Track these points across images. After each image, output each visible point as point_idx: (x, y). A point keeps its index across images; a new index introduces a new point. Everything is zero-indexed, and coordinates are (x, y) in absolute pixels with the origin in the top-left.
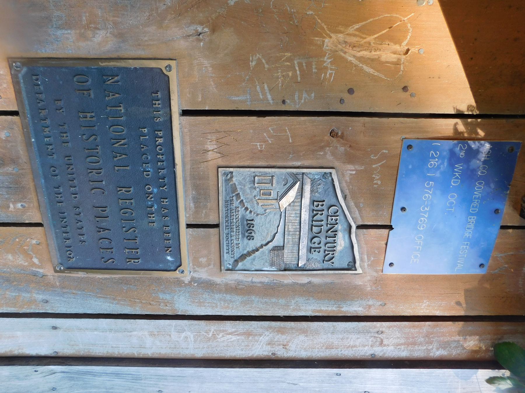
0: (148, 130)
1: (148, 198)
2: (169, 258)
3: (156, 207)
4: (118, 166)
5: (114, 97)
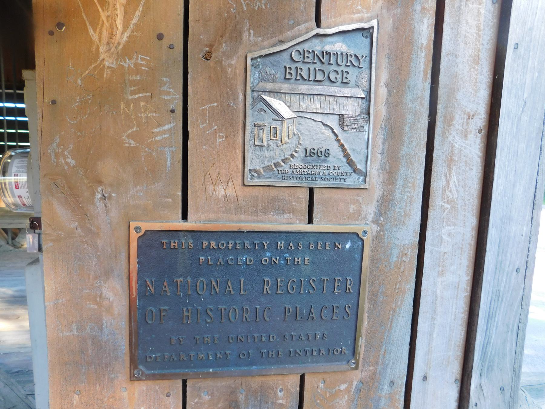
0: (202, 256)
1: (277, 262)
2: (347, 246)
3: (288, 255)
5: (167, 286)
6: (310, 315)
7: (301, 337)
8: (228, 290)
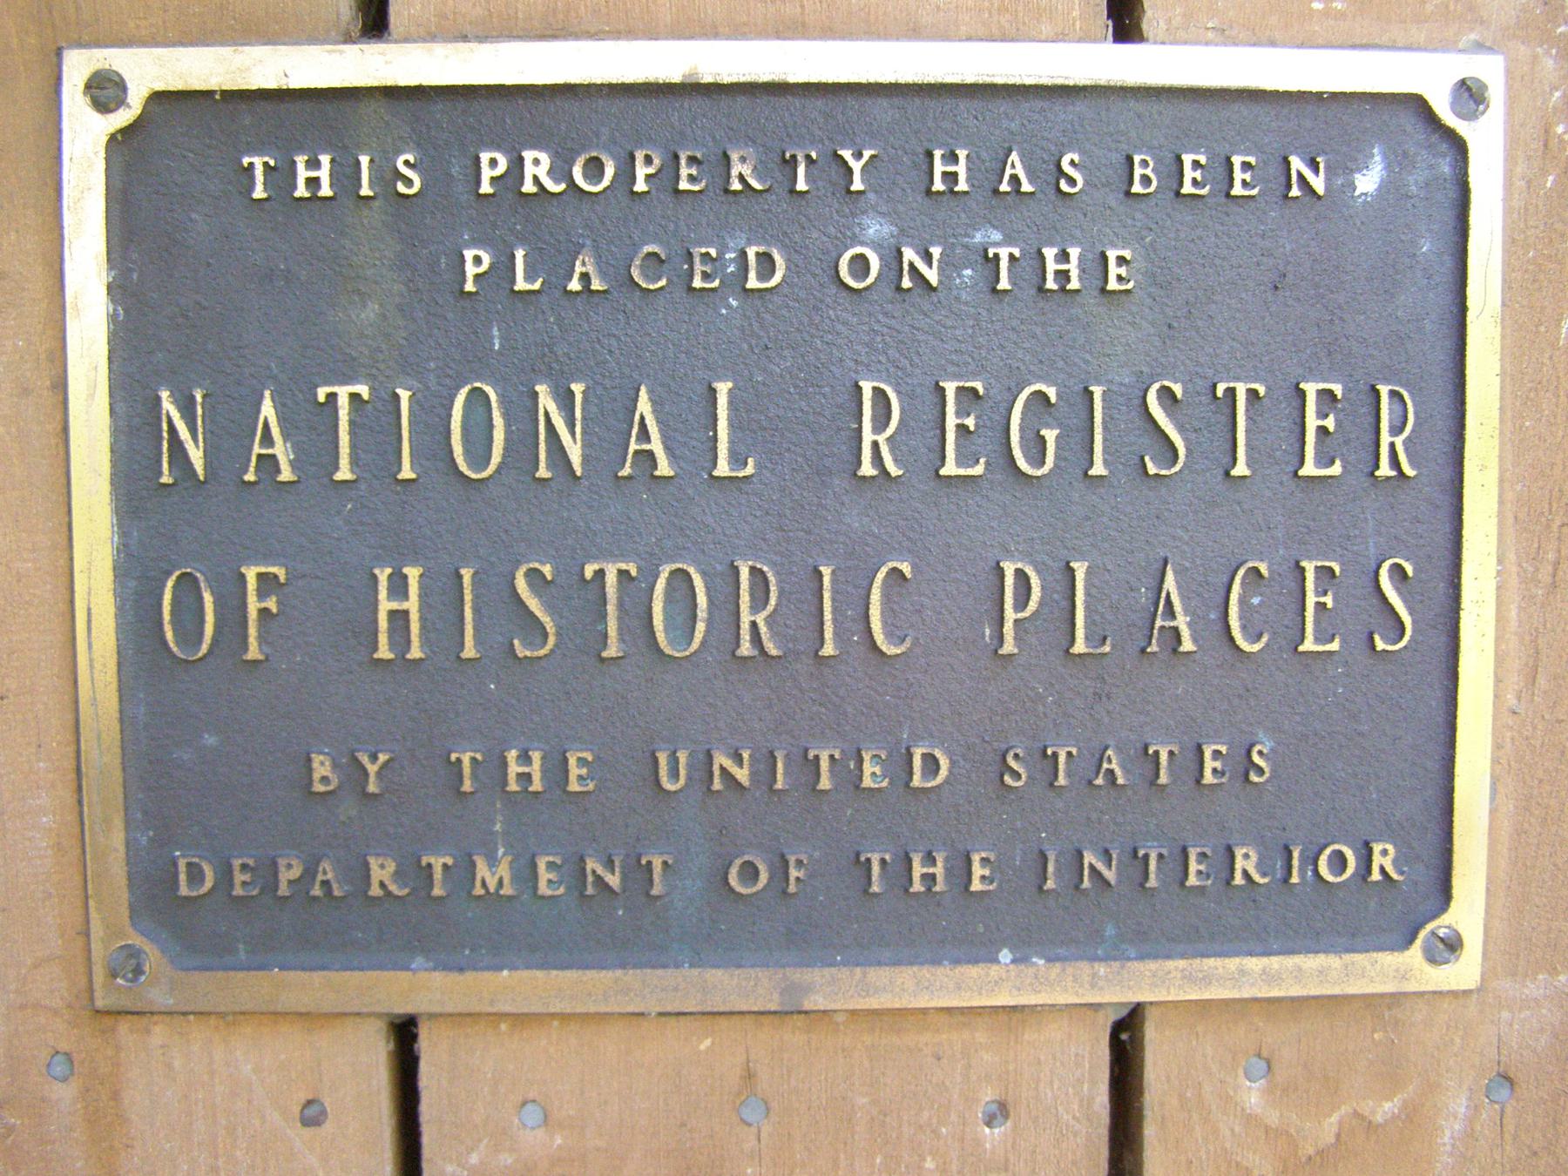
0: (475, 243)
1: (932, 276)
2: (1367, 182)
3: (996, 236)
4: (1370, 458)
5: (275, 431)
6: (1159, 623)
7: (1105, 766)
8: (637, 452)
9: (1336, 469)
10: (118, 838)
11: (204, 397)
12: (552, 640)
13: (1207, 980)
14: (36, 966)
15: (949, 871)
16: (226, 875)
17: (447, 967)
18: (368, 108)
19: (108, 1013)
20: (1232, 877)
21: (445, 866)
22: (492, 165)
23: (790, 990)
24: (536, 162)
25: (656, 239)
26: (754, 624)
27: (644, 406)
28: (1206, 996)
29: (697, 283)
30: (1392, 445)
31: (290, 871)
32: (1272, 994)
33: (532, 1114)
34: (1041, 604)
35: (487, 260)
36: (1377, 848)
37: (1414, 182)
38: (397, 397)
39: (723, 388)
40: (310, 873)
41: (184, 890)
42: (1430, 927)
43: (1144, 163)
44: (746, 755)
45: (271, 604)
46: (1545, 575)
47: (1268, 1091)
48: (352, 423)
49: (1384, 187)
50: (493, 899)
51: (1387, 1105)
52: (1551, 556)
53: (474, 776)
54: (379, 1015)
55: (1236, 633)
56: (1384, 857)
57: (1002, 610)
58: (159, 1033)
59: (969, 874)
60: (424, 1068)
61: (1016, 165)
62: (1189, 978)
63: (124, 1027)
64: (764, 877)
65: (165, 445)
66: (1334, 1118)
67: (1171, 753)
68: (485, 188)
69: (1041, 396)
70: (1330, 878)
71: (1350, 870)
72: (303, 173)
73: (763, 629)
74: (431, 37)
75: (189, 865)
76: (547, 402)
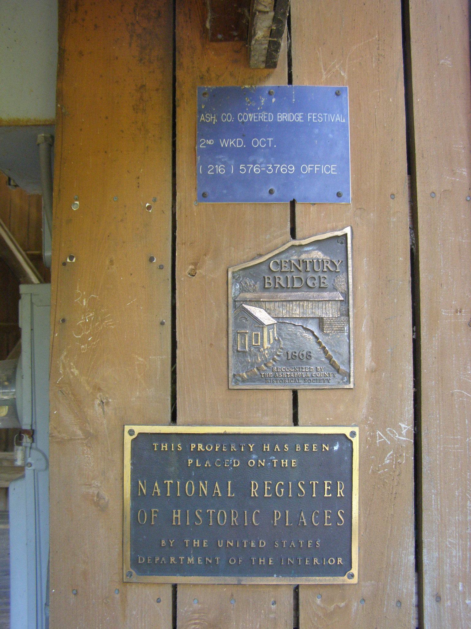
1: (263, 464)
2: (336, 448)
6: (300, 521)
9: (330, 495)
10: (129, 553)
11: (146, 482)
12: (201, 522)
13: (309, 581)
14: (114, 574)
15: (265, 561)
16: (147, 559)
17: (183, 576)
18: (173, 436)
19: (126, 582)
20: (313, 563)
21: (183, 559)
22: (193, 446)
23: (239, 580)
24: (200, 446)
25: (218, 458)
26: (234, 520)
27: (217, 485)
28: (309, 583)
29: (225, 465)
30: (340, 491)
31: (157, 559)
32: (321, 583)
33: (196, 601)
34: (281, 517)
35: (192, 461)
36: (339, 559)
37: (344, 448)
38: (177, 483)
39: (229, 482)
40: (161, 559)
41: (139, 562)
42: (348, 572)
43: (298, 446)
44: (232, 541)
45: (156, 515)
46: (368, 512)
47: (321, 601)
48: (170, 486)
49: (339, 448)
50: (190, 564)
51: (342, 604)
52: (369, 509)
53: (188, 544)
54: (171, 584)
55: (314, 522)
56: (340, 560)
57: (274, 518)
58: (134, 586)
59: (269, 562)
60: (178, 593)
61: (277, 447)
62: (306, 580)
63: (128, 585)
64: (235, 561)
65: (139, 489)
66: (333, 606)
67: (303, 542)
68: (192, 450)
69: (281, 484)
70: (330, 564)
71: (334, 562)
72: (163, 447)
73: (235, 521)
74: (183, 425)
75: (141, 558)
76: (201, 484)
